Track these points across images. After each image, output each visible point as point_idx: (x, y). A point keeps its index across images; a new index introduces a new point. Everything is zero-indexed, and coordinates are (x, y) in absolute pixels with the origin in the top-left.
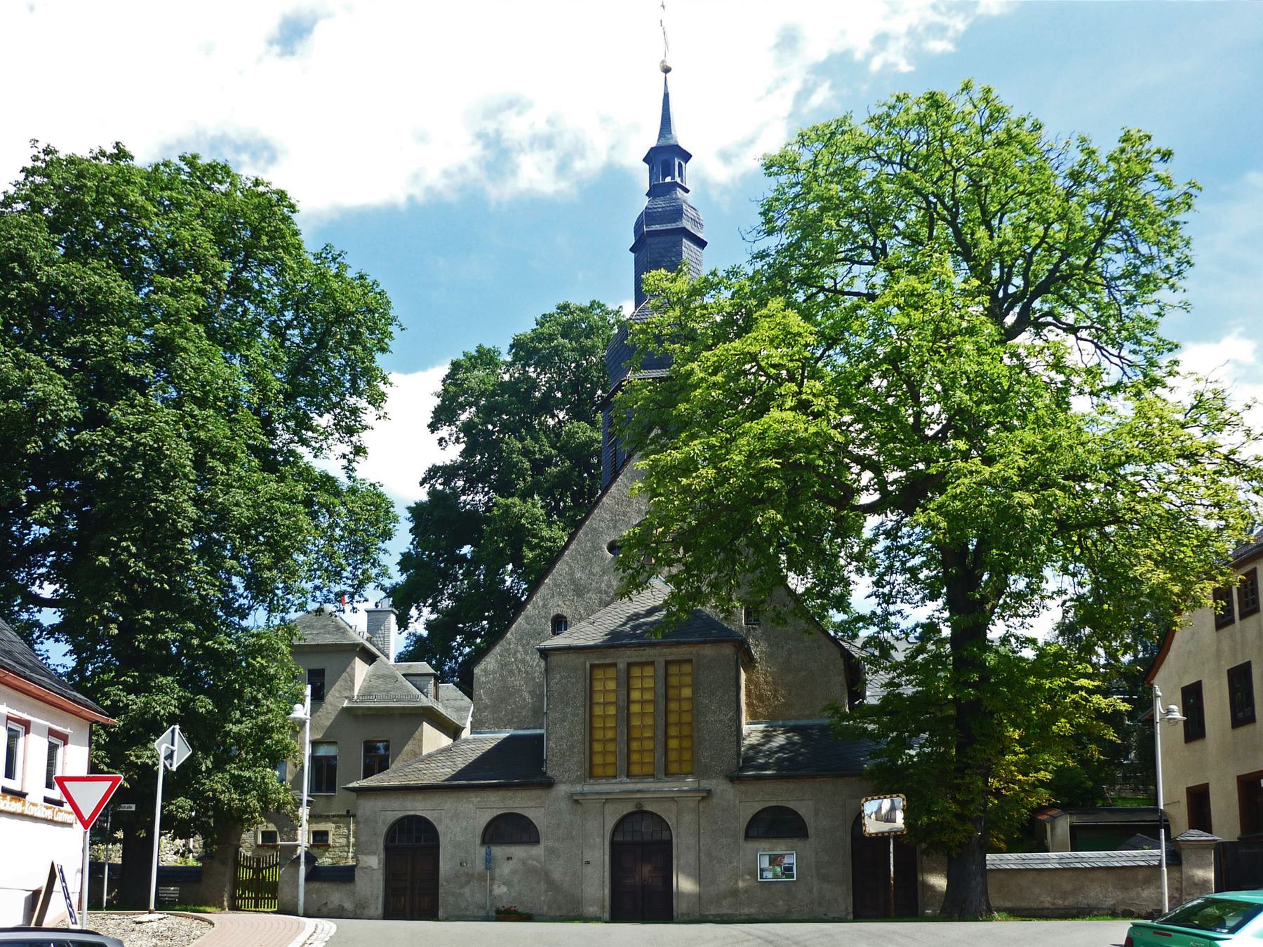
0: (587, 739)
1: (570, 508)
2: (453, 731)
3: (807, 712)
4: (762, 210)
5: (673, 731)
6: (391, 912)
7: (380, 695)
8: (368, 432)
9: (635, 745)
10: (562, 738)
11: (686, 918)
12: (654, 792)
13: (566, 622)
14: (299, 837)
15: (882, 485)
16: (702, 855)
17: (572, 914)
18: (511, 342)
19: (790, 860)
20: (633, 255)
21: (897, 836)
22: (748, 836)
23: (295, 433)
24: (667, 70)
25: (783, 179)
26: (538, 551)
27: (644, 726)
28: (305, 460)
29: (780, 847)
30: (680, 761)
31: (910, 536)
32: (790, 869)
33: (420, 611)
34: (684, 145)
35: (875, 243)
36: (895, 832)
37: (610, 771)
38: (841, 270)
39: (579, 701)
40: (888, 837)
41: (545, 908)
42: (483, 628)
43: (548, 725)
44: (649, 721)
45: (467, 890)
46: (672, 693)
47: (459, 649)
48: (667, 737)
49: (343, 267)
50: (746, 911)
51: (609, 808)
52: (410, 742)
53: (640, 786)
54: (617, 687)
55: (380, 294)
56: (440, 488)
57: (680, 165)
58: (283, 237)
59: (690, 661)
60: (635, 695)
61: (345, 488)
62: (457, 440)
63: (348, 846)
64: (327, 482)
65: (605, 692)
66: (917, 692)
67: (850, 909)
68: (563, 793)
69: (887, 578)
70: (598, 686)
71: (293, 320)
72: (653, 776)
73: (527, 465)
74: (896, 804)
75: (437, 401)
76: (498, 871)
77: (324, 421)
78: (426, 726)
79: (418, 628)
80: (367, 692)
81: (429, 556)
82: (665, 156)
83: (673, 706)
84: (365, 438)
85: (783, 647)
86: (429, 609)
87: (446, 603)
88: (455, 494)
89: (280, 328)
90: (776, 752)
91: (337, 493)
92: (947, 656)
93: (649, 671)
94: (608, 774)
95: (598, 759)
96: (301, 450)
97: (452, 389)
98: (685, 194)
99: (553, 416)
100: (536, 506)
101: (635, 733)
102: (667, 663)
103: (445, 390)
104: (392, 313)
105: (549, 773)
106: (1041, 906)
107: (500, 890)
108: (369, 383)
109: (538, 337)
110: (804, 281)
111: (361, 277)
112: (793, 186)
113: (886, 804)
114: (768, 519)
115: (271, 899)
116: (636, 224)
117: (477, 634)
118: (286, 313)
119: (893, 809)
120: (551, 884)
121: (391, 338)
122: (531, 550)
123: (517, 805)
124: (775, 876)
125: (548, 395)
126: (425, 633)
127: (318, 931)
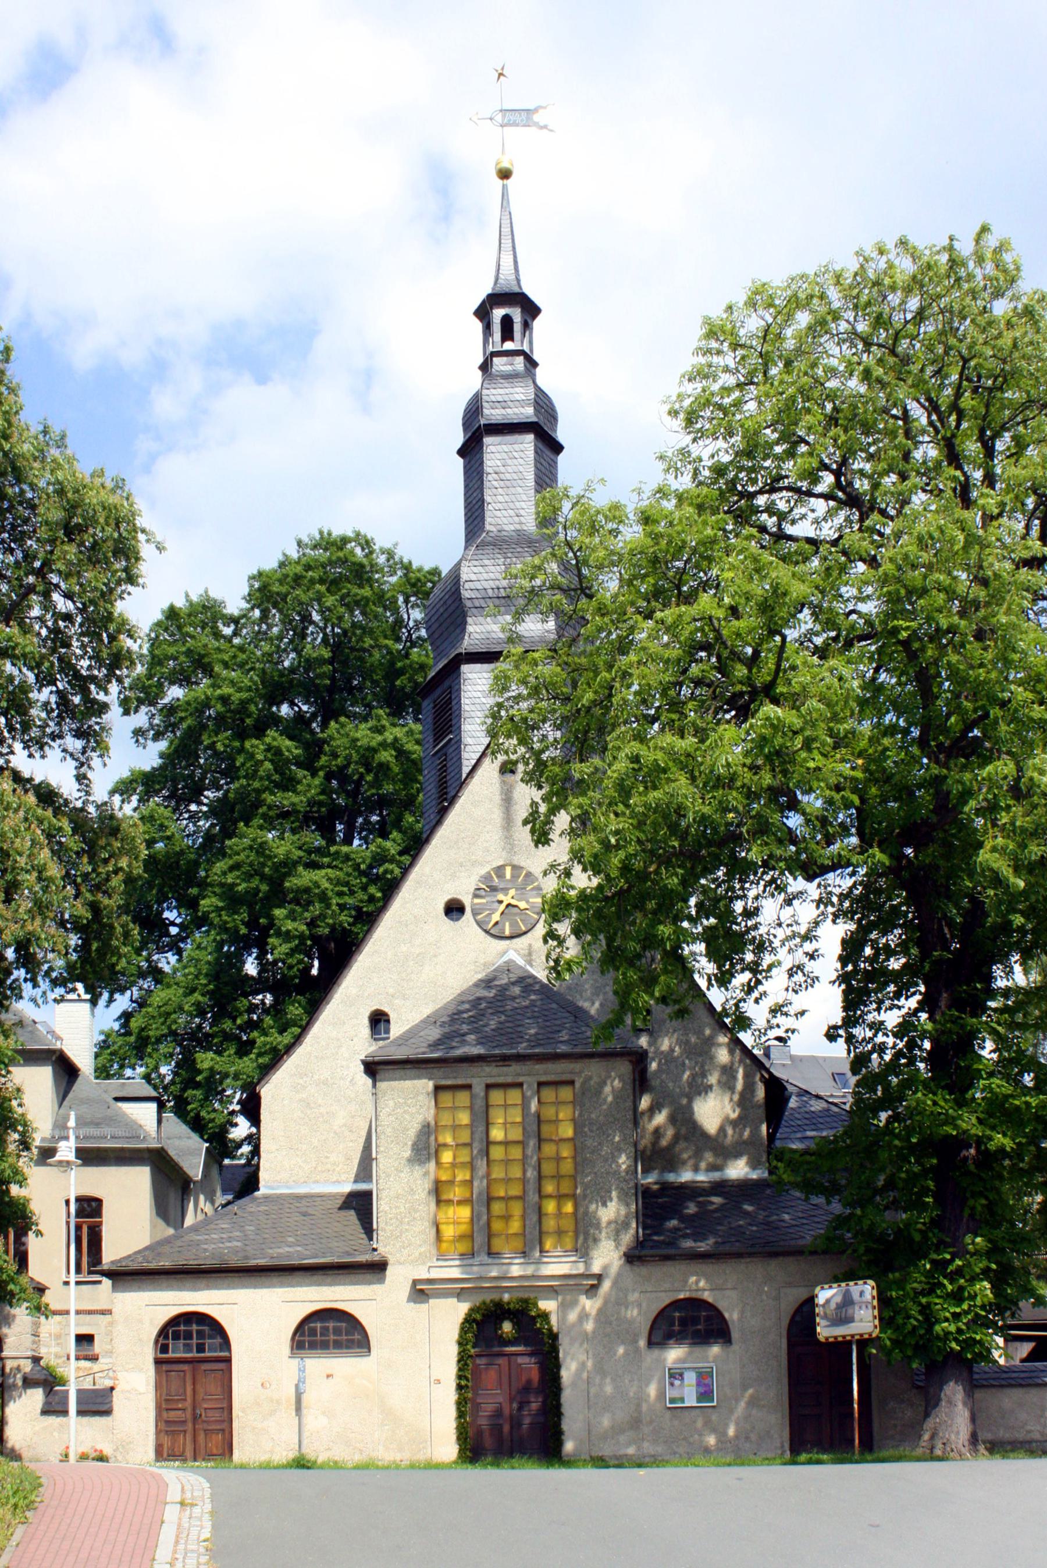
5: (549, 1188)
13: (388, 1021)
24: (505, 174)
36: (861, 1335)
46: (546, 1129)
54: (473, 1121)
60: (497, 1134)
106: (1028, 1437)
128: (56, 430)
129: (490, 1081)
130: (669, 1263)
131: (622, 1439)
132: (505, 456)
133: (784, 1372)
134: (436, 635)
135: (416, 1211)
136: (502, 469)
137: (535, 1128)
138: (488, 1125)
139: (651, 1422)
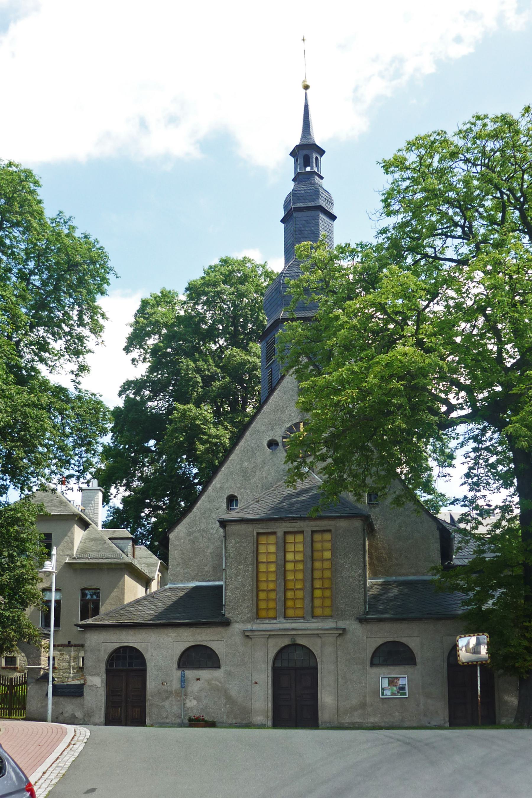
0: (255, 590)
1: (228, 412)
2: (146, 582)
3: (413, 571)
4: (383, 198)
5: (317, 584)
6: (110, 721)
7: (94, 554)
8: (90, 354)
9: (290, 594)
10: (236, 588)
11: (328, 725)
12: (279, 630)
13: (237, 500)
14: (42, 663)
15: (472, 401)
16: (339, 677)
17: (245, 722)
18: (187, 286)
19: (403, 682)
20: (283, 225)
21: (483, 665)
22: (372, 664)
23: (36, 354)
24: (306, 87)
25: (397, 176)
26: (207, 445)
27: (296, 580)
28: (43, 375)
29: (394, 671)
30: (323, 607)
31: (491, 439)
32: (403, 688)
33: (118, 490)
34: (318, 142)
35: (465, 223)
36: (482, 662)
37: (272, 613)
38: (438, 243)
39: (249, 560)
40: (476, 666)
41: (225, 717)
42: (165, 504)
43: (226, 578)
44: (300, 576)
45: (167, 704)
46: (317, 555)
47: (147, 519)
48: (313, 589)
49: (72, 228)
50: (372, 720)
51: (271, 642)
52: (115, 590)
53: (294, 626)
54: (277, 550)
55: (100, 249)
56: (132, 396)
57: (317, 158)
58: (30, 206)
59: (329, 531)
60: (290, 556)
61: (73, 397)
62: (144, 360)
63: (69, 669)
64: (60, 391)
65: (268, 553)
66: (496, 557)
67: (447, 719)
68: (237, 630)
69: (474, 472)
70: (262, 549)
71: (35, 268)
72: (303, 618)
73: (199, 379)
74: (481, 640)
75: (131, 330)
76: (190, 689)
77: (58, 345)
78: (127, 578)
79: (117, 502)
80: (83, 551)
81: (124, 448)
82: (305, 152)
83: (317, 565)
84: (88, 359)
85: (395, 521)
86: (124, 488)
87: (136, 484)
88: (144, 402)
89: (26, 275)
90: (391, 601)
91: (68, 400)
92: (517, 530)
93: (300, 538)
94: (270, 616)
95: (262, 605)
96: (40, 367)
97: (142, 320)
98: (321, 181)
99: (215, 343)
100: (207, 410)
101: (290, 585)
102: (313, 532)
103: (137, 322)
104: (110, 264)
105: (227, 615)
107: (191, 703)
108: (91, 318)
109: (207, 284)
110: (412, 250)
111: (86, 237)
112: (404, 180)
113: (473, 640)
114: (396, 426)
115: (21, 709)
116: (285, 202)
117: (160, 508)
118: (30, 263)
119: (478, 644)
120: (229, 699)
121: (108, 284)
122: (202, 444)
123: (204, 639)
124: (393, 694)
125: (212, 328)
126: (121, 507)
127: (78, 735)
128: (67, 215)
129: (286, 530)
130: (381, 623)
131: (356, 714)
132: (304, 222)
133: (446, 680)
134: (268, 310)
135: (246, 595)
136: (303, 229)
137: (310, 554)
138: (285, 552)
139: (372, 705)
